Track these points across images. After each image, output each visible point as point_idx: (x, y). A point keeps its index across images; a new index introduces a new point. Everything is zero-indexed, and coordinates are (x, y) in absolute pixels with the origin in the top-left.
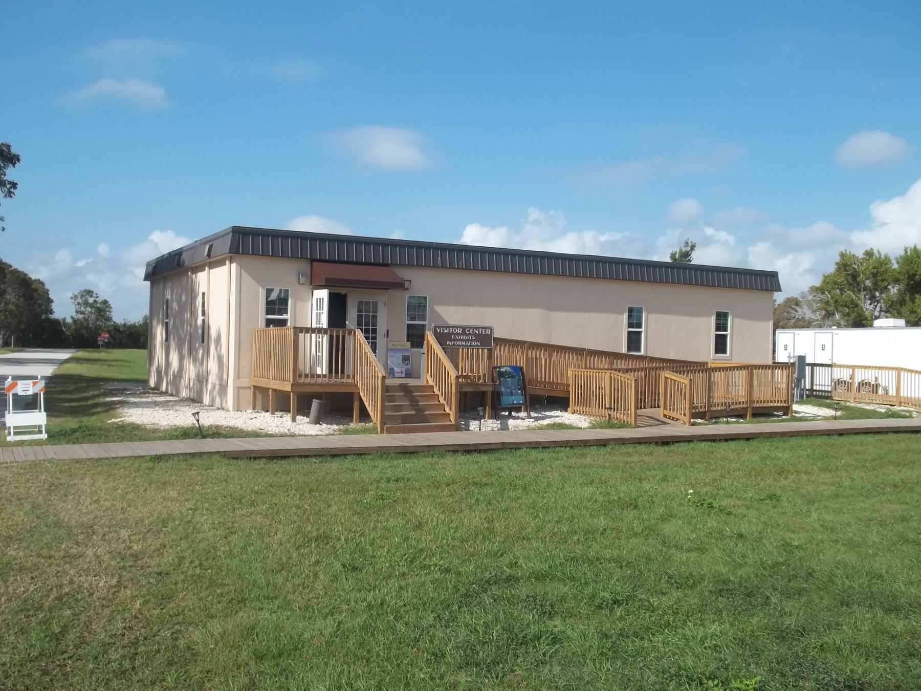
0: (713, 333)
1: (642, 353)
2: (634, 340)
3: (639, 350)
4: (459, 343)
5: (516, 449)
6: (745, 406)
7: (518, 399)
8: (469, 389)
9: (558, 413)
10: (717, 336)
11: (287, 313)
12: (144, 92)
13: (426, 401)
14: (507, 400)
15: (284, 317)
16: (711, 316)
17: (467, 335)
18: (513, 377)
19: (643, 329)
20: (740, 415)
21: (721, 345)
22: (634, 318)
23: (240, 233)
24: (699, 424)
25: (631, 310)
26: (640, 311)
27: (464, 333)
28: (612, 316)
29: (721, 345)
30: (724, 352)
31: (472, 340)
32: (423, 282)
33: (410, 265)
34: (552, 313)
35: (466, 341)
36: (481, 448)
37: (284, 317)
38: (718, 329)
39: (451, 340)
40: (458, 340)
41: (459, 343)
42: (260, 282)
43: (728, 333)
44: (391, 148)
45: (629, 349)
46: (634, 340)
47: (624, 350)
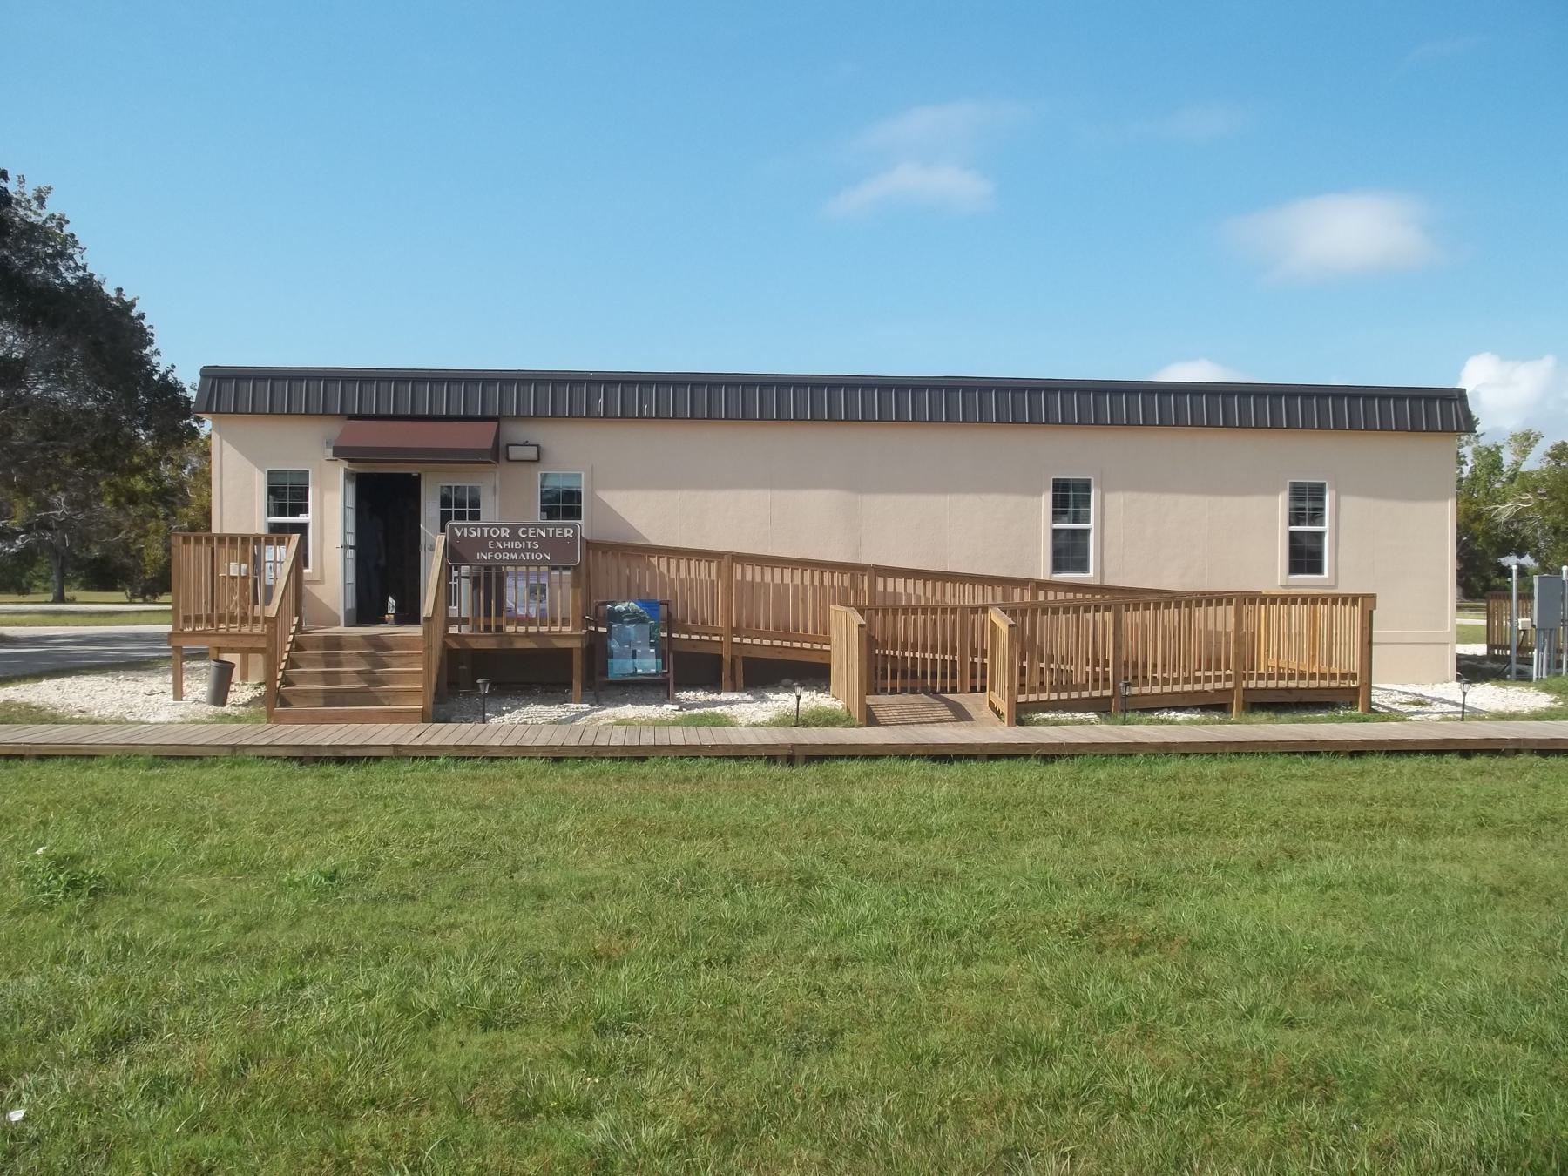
0: (1282, 529)
1: (1090, 576)
2: (1069, 551)
3: (1082, 566)
4: (505, 556)
5: (692, 758)
6: (1230, 685)
7: (648, 664)
8: (455, 646)
9: (701, 695)
10: (1293, 537)
11: (306, 512)
12: (955, 184)
13: (405, 665)
14: (620, 667)
15: (301, 519)
16: (1275, 492)
17: (521, 540)
18: (642, 621)
19: (1091, 525)
20: (1215, 705)
21: (1305, 556)
22: (1069, 498)
23: (214, 377)
24: (1089, 722)
25: (1298, 491)
26: (1318, 491)
27: (514, 536)
28: (1012, 500)
29: (1305, 556)
30: (1317, 568)
31: (532, 550)
32: (572, 451)
33: (538, 416)
34: (866, 499)
35: (519, 551)
36: (348, 753)
37: (301, 519)
38: (1296, 517)
39: (486, 550)
40: (501, 551)
41: (505, 556)
42: (256, 461)
43: (1326, 527)
44: (1350, 229)
45: (1057, 566)
46: (1069, 551)
47: (1044, 571)
